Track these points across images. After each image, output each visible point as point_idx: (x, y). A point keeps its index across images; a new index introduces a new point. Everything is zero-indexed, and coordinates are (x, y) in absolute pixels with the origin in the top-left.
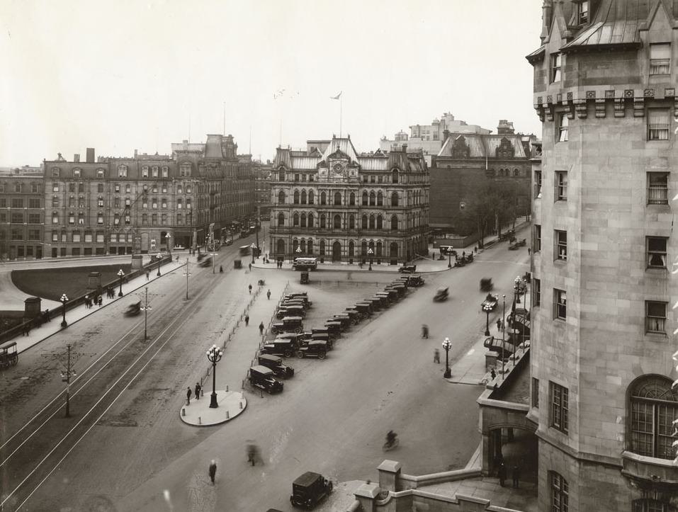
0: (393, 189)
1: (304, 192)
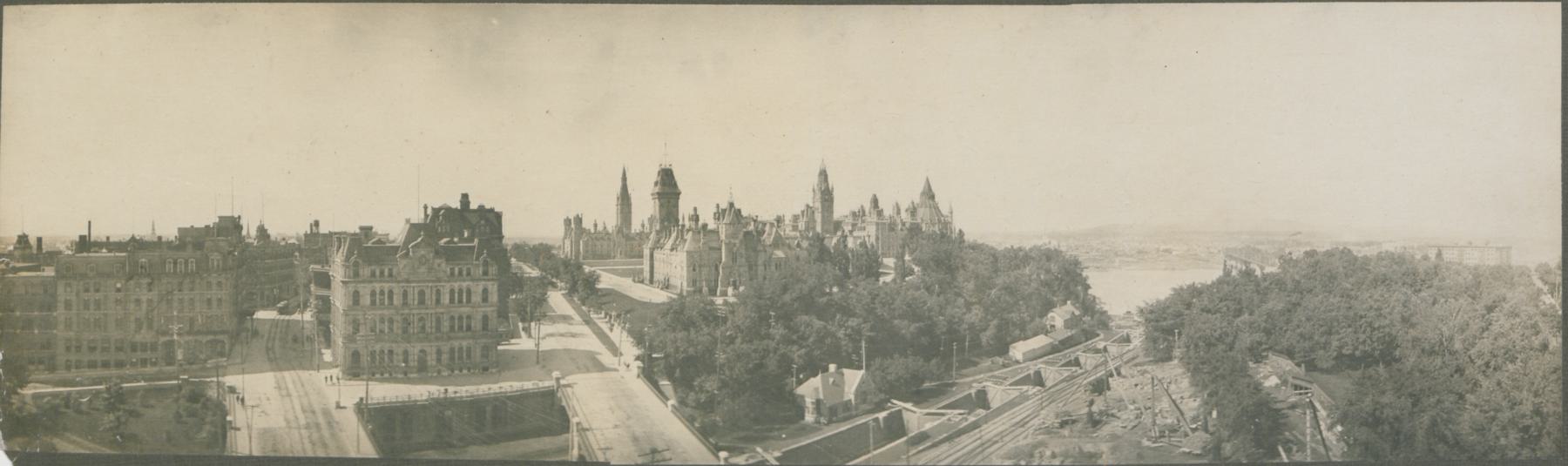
0: (483, 283)
1: (461, 349)
